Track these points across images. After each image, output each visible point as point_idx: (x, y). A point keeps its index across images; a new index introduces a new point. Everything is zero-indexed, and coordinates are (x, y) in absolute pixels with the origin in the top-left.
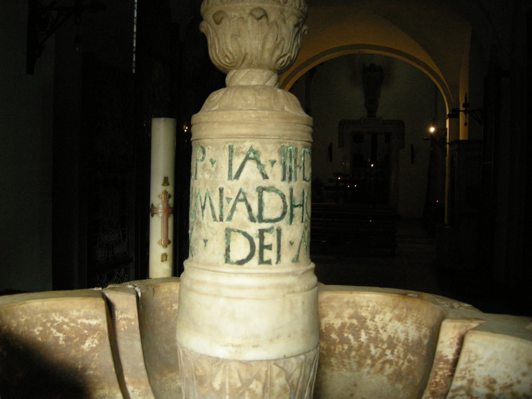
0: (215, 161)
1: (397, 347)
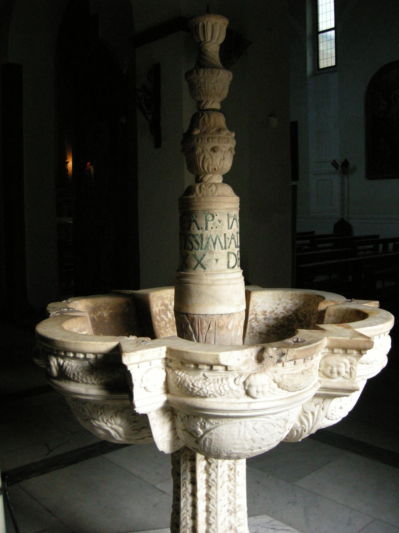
0: (221, 221)
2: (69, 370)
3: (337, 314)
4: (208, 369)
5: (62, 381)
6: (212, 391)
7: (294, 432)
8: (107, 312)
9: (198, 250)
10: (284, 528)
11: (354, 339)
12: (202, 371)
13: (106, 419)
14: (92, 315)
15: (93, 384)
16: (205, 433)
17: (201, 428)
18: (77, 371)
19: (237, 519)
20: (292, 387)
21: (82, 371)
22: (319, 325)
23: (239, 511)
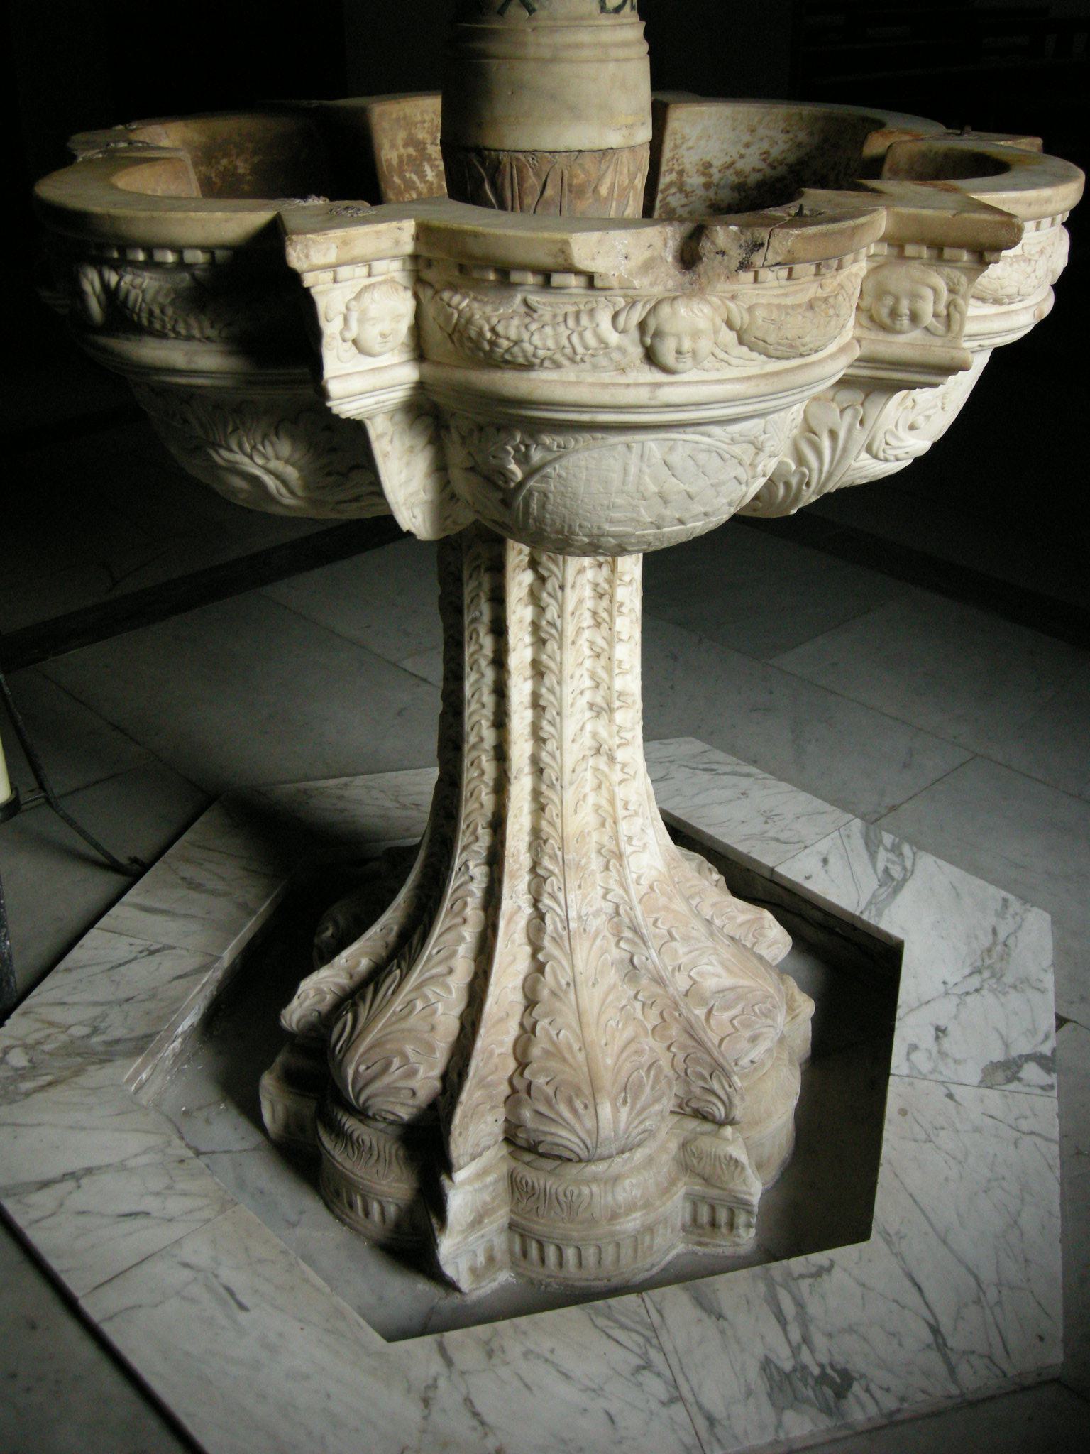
2: (136, 301)
4: (537, 285)
5: (118, 337)
6: (549, 349)
7: (777, 486)
8: (246, 161)
10: (738, 769)
11: (966, 215)
12: (521, 291)
13: (249, 443)
14: (203, 169)
15: (208, 338)
16: (528, 477)
17: (518, 462)
18: (160, 304)
19: (615, 729)
20: (779, 344)
21: (173, 303)
22: (864, 181)
23: (620, 708)
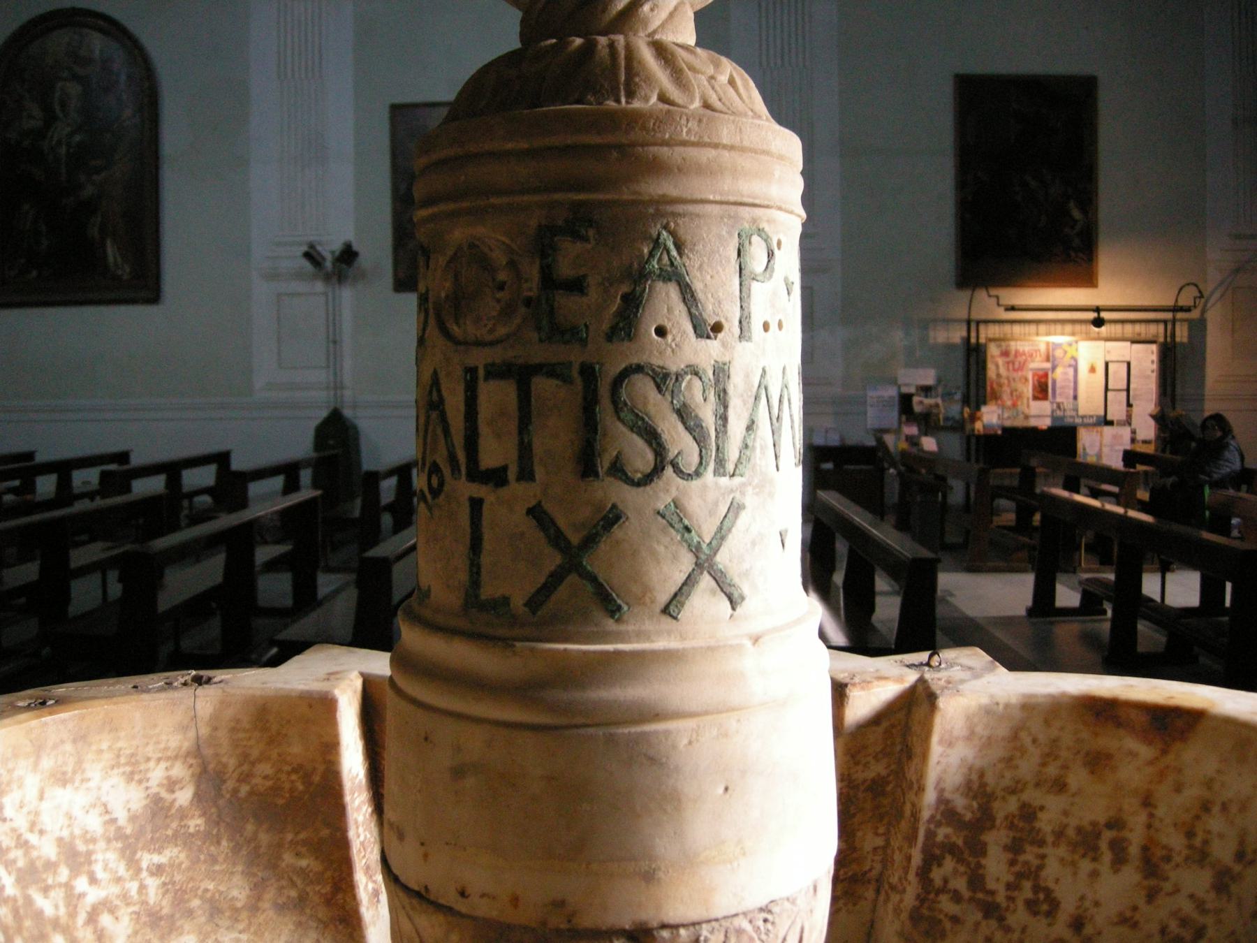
1: (93, 858)
3: (979, 729)
9: (698, 474)
